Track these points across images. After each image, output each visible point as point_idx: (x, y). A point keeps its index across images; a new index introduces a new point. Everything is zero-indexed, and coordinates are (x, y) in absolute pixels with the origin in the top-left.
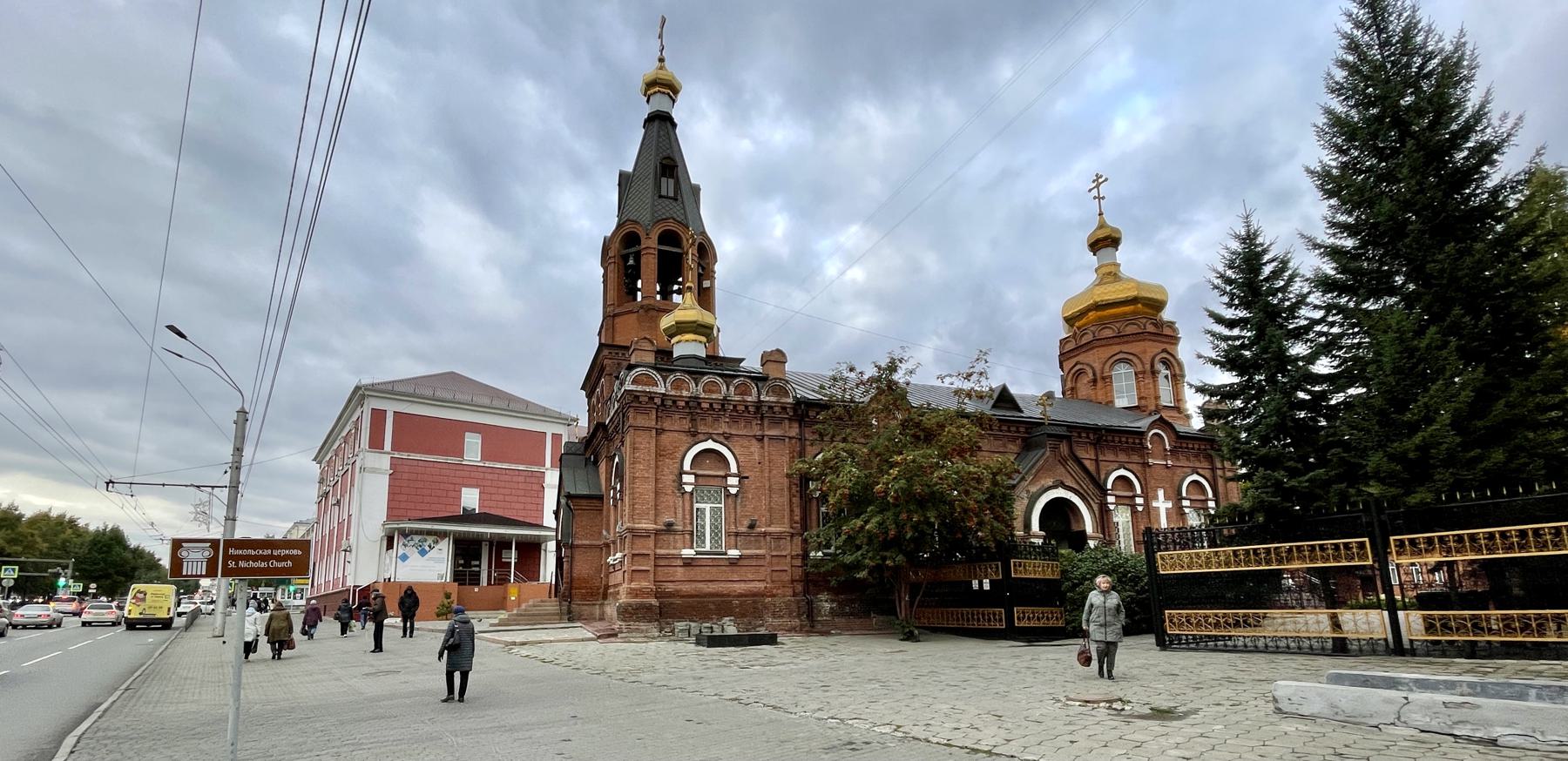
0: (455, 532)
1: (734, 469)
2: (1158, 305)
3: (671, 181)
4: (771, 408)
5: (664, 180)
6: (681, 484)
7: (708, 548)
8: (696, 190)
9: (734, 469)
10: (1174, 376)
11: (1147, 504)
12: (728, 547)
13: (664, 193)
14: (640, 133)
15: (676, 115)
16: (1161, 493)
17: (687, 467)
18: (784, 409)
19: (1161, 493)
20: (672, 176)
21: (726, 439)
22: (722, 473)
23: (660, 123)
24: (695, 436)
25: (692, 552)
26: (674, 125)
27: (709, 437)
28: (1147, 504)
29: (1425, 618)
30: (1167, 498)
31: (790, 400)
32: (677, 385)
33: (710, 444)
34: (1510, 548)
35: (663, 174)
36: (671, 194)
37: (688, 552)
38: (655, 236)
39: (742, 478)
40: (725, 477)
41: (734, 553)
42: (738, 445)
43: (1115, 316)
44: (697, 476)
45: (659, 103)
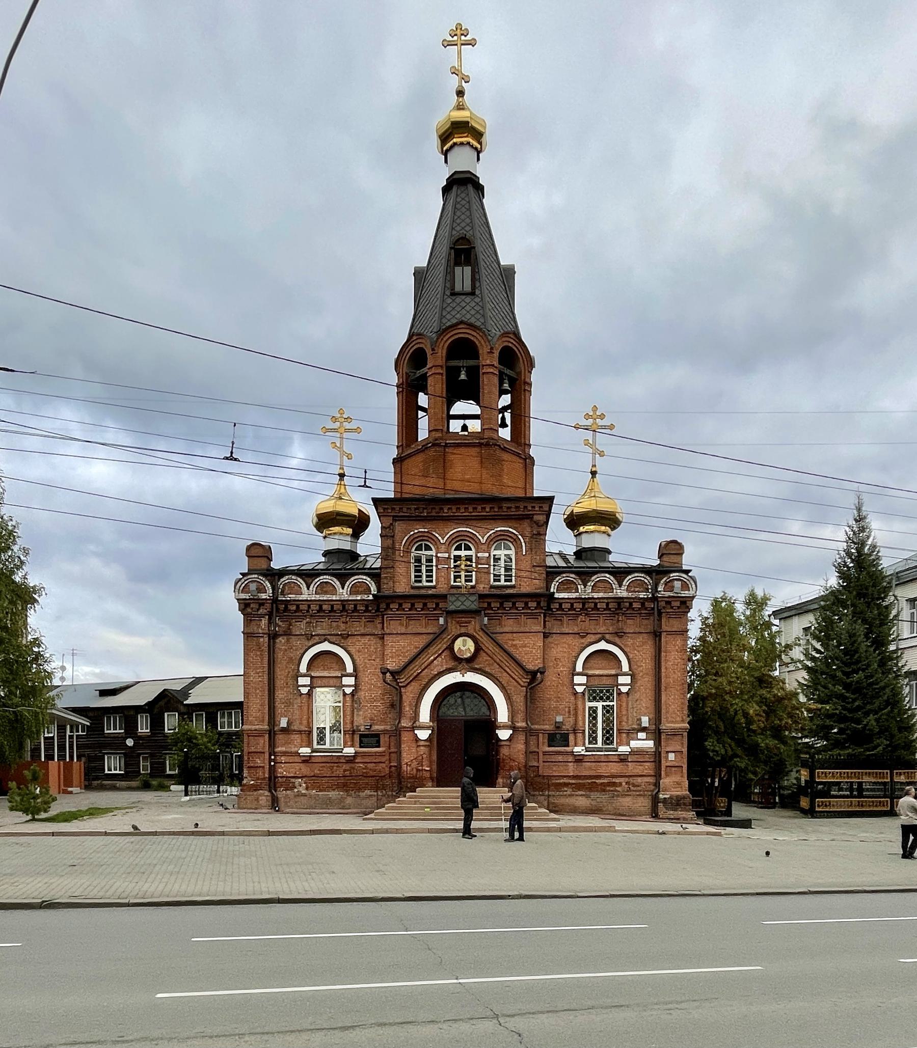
1: (625, 667)
3: (468, 270)
5: (458, 270)
7: (327, 746)
8: (508, 275)
9: (625, 667)
13: (458, 288)
14: (438, 201)
15: (482, 172)
20: (468, 262)
21: (342, 639)
22: (613, 672)
23: (463, 187)
24: (311, 639)
25: (308, 750)
26: (479, 189)
27: (324, 639)
32: (323, 588)
33: (326, 646)
35: (457, 263)
36: (468, 287)
37: (305, 751)
38: (442, 352)
39: (633, 676)
40: (617, 675)
41: (349, 751)
42: (357, 644)
45: (462, 160)
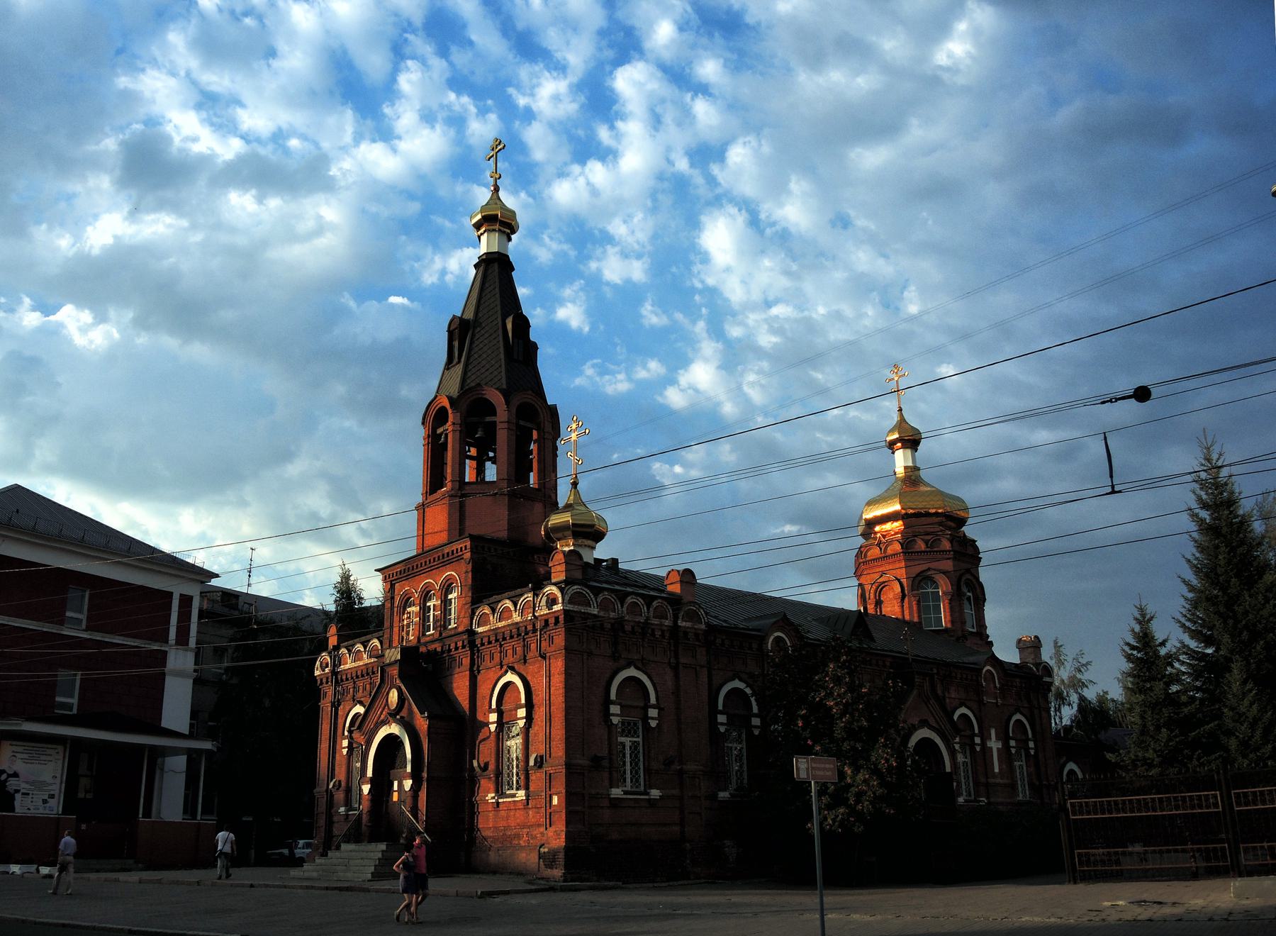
0: (189, 749)
2: (962, 522)
4: (686, 633)
6: (607, 714)
7: (628, 788)
10: (976, 598)
11: (983, 744)
12: (649, 786)
16: (993, 732)
17: (613, 696)
18: (697, 635)
19: (993, 732)
28: (983, 744)
29: (13, 810)
30: (998, 738)
31: (703, 627)
34: (1193, 807)
39: (661, 709)
43: (22, 533)
44: (622, 707)
